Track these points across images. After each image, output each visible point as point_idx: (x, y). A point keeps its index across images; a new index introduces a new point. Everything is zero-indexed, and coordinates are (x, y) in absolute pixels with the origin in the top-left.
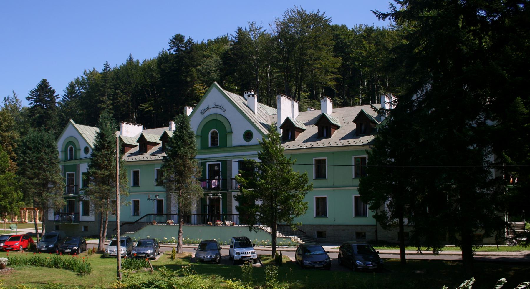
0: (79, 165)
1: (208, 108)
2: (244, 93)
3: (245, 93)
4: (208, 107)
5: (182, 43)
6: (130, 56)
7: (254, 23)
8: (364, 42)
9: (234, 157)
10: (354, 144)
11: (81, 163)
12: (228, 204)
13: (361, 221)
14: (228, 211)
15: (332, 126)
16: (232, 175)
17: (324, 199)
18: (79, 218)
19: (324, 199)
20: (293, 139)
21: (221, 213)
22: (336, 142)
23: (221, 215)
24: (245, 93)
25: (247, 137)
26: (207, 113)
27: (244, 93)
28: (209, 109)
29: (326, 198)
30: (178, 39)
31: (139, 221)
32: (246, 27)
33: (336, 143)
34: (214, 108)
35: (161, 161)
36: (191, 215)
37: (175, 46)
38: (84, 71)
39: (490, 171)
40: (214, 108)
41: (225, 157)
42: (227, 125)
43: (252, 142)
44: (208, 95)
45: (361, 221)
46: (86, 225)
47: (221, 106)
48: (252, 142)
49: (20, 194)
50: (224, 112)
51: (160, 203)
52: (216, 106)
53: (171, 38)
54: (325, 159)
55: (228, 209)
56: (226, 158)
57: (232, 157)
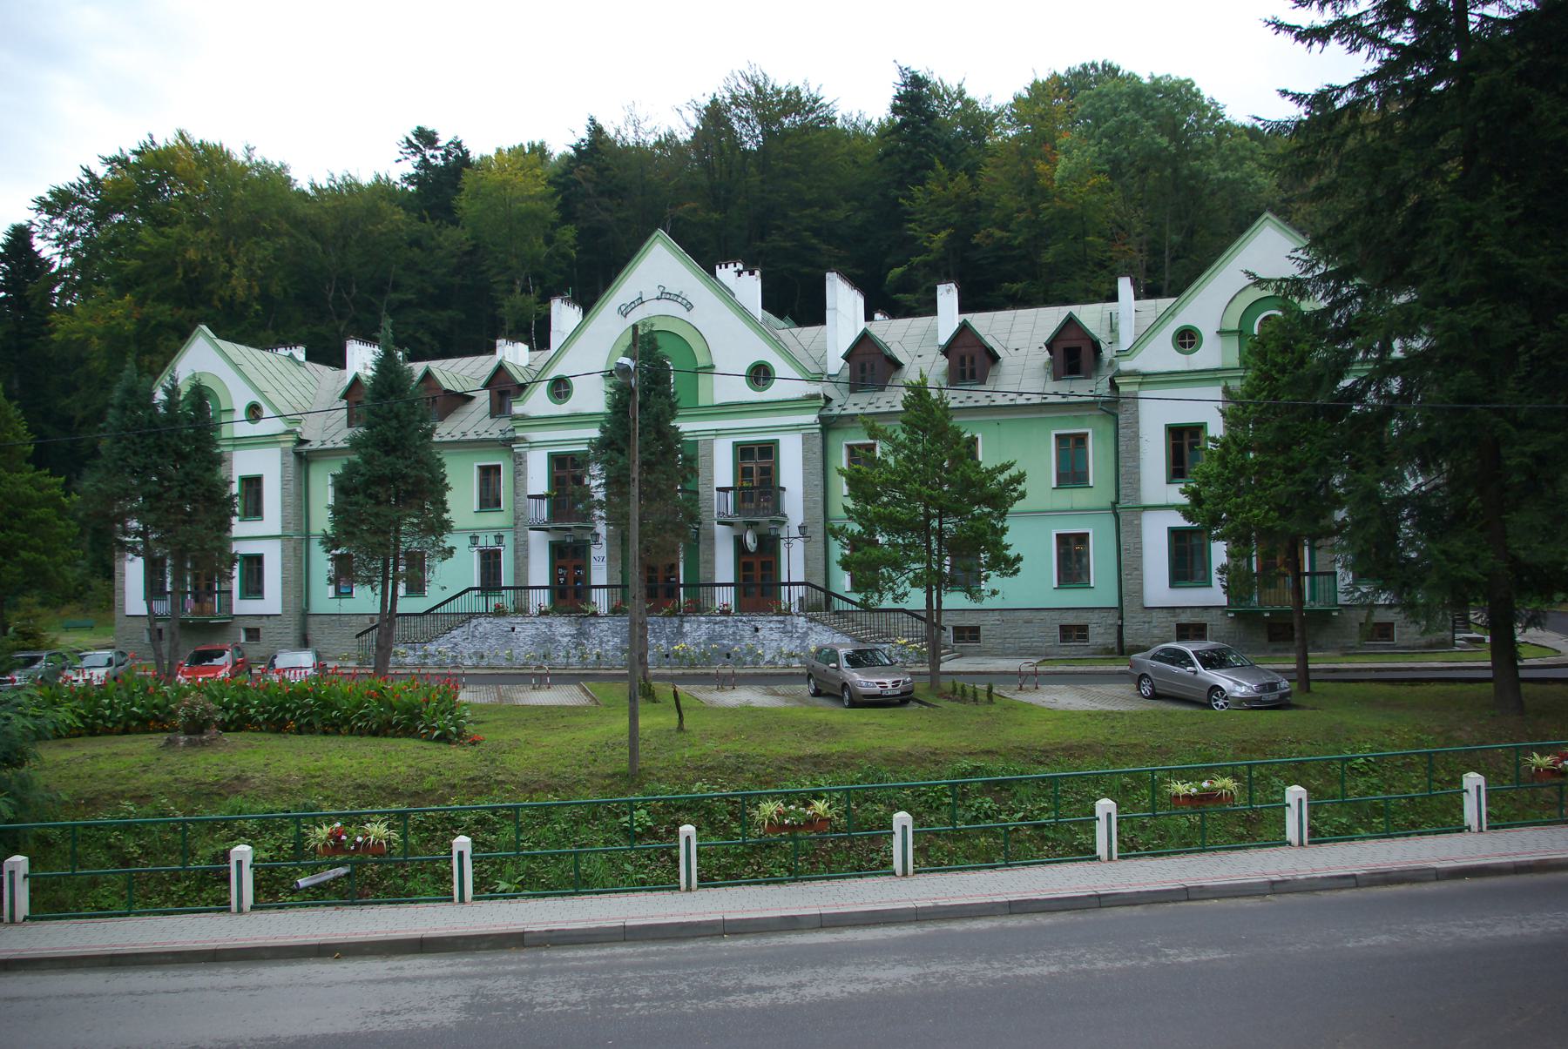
1: (641, 301)
4: (641, 298)
6: (593, 121)
13: (1074, 597)
17: (1082, 538)
18: (230, 605)
19: (1082, 538)
21: (681, 582)
23: (1307, 574)
26: (636, 316)
27: (717, 267)
28: (643, 302)
29: (1057, 535)
31: (439, 610)
34: (658, 299)
38: (1270, 30)
39: (446, 521)
42: (697, 347)
43: (767, 395)
45: (1074, 597)
46: (253, 624)
47: (679, 296)
50: (688, 310)
52: (664, 296)
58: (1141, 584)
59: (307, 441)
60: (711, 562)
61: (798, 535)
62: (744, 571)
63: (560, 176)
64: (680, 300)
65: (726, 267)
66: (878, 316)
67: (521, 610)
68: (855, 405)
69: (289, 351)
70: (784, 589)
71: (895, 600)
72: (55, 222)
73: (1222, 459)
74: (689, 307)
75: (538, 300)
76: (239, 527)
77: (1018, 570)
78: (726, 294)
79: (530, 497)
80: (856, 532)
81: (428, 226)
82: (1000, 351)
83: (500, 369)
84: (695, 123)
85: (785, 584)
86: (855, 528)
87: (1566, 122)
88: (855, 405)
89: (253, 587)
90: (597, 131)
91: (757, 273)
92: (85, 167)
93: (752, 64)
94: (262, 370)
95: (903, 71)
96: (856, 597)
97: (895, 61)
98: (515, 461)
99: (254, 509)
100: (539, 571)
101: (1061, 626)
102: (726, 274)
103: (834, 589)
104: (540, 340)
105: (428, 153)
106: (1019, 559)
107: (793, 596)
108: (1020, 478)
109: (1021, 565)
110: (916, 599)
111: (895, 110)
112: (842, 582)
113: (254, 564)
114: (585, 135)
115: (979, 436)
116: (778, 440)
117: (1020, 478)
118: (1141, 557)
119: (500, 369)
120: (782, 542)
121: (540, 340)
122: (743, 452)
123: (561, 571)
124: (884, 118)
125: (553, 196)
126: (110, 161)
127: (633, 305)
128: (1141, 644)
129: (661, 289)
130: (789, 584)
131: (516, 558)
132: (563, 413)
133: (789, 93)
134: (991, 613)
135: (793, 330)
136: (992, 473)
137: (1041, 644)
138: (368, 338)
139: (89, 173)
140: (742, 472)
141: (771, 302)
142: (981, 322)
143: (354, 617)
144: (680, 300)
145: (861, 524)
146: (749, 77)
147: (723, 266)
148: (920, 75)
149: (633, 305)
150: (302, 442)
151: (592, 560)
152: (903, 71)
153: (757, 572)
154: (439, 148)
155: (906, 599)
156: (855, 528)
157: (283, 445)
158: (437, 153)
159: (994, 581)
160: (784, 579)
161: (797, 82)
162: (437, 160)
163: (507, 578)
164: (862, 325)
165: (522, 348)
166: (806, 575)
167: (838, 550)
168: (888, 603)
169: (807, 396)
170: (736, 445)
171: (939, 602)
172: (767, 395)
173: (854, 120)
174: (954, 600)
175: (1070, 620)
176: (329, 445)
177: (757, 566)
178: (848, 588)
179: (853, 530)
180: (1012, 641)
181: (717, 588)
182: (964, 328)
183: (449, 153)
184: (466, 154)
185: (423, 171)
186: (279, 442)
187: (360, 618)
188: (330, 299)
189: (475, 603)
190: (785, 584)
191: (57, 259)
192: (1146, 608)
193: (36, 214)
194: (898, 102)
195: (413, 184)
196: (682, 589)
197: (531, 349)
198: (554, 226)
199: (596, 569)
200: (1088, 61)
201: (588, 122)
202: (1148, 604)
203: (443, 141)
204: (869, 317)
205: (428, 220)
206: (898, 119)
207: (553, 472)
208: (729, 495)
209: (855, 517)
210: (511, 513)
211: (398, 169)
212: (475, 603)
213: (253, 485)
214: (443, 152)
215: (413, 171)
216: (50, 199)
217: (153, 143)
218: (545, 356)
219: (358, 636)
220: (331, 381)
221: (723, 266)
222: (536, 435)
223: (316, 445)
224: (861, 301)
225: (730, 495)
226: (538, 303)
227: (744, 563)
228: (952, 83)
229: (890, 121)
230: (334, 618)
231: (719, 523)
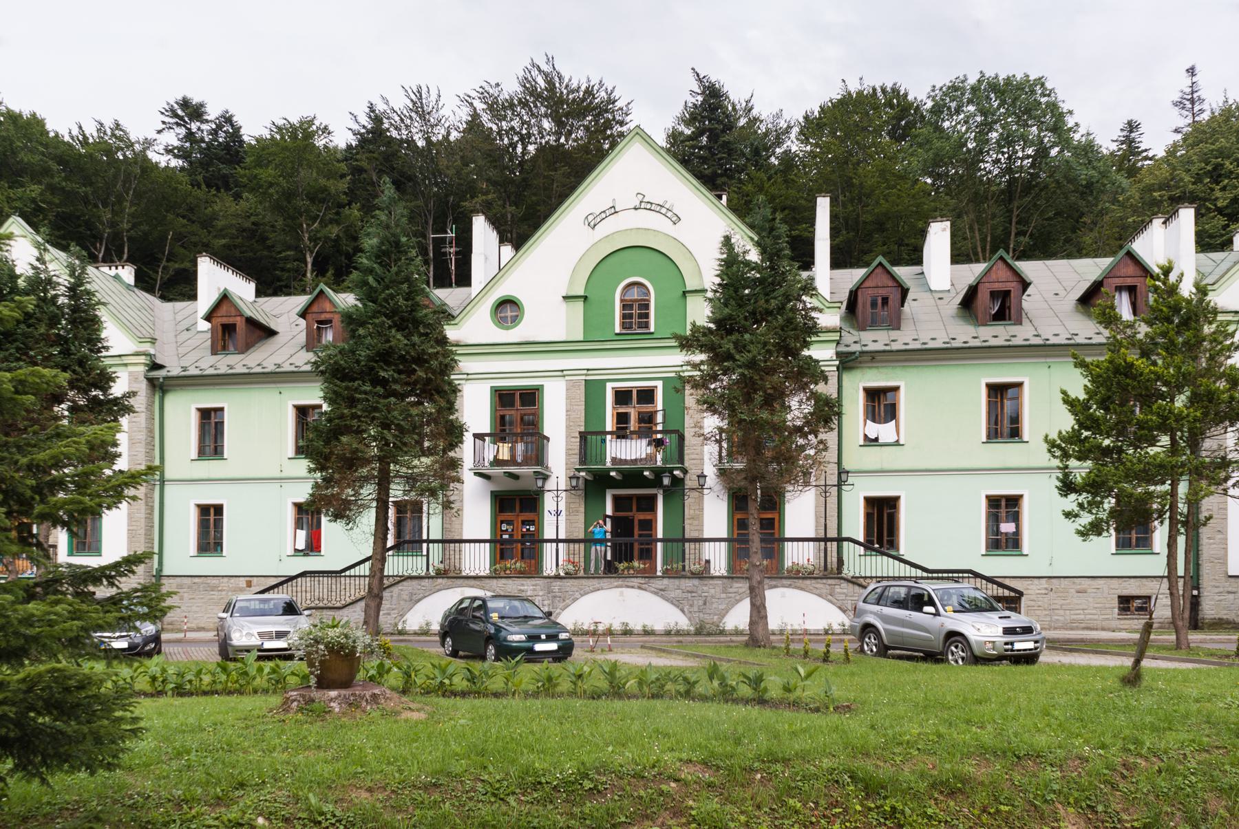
10: (999, 342)
21: (660, 535)
31: (352, 572)
34: (636, 209)
52: (645, 205)
58: (1226, 549)
64: (664, 211)
69: (113, 272)
73: (330, 420)
74: (677, 220)
87: (1238, 149)
93: (550, 57)
101: (1119, 597)
105: (194, 126)
107: (798, 555)
115: (902, 384)
118: (1226, 519)
122: (503, 398)
123: (504, 527)
127: (603, 215)
128: (1225, 617)
129: (640, 197)
130: (429, 541)
134: (1036, 581)
137: (1096, 617)
143: (226, 580)
144: (664, 211)
149: (603, 215)
150: (155, 366)
151: (546, 513)
154: (207, 121)
157: (131, 368)
158: (205, 127)
162: (203, 130)
175: (1131, 589)
176: (193, 371)
180: (1061, 612)
183: (219, 127)
184: (237, 130)
185: (188, 144)
186: (126, 365)
187: (233, 580)
192: (1231, 577)
196: (659, 545)
202: (1230, 573)
203: (213, 112)
215: (176, 143)
223: (175, 371)
230: (196, 580)
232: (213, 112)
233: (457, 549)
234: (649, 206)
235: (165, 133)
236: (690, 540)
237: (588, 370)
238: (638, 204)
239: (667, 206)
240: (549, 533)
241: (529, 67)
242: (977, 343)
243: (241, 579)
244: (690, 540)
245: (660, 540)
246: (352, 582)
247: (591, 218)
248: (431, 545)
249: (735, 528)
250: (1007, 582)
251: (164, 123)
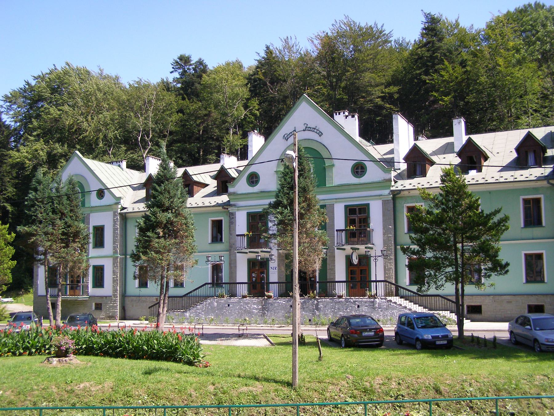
0: (89, 215)
2: (335, 114)
3: (336, 115)
4: (295, 130)
5: (189, 64)
7: (289, 38)
8: (446, 63)
9: (338, 200)
10: (522, 178)
11: (92, 212)
12: (328, 268)
14: (328, 277)
15: (427, 162)
16: (334, 225)
19: (539, 257)
20: (423, 174)
21: (318, 280)
22: (428, 183)
24: (336, 115)
25: (357, 172)
27: (335, 114)
29: (526, 255)
30: (184, 60)
32: (277, 45)
33: (429, 184)
34: (304, 130)
35: (221, 208)
36: (269, 283)
37: (179, 68)
40: (304, 130)
41: (324, 200)
43: (364, 180)
44: (295, 114)
46: (99, 301)
48: (364, 179)
49: (490, 265)
50: (320, 136)
51: (217, 269)
52: (307, 128)
53: (176, 59)
54: (408, 207)
55: (328, 274)
56: (326, 201)
57: (335, 200)
59: (126, 208)
60: (333, 270)
61: (381, 254)
62: (351, 275)
63: (252, 76)
65: (339, 114)
66: (420, 138)
67: (233, 295)
68: (410, 184)
70: (373, 285)
71: (437, 288)
72: (13, 106)
74: (320, 134)
75: (241, 137)
76: (93, 252)
77: (507, 271)
78: (341, 130)
79: (238, 235)
80: (416, 250)
81: (187, 102)
82: (489, 154)
83: (222, 169)
84: (320, 47)
85: (374, 281)
86: (415, 247)
88: (410, 184)
89: (99, 282)
90: (269, 51)
91: (356, 117)
92: (27, 81)
93: (346, 15)
94: (105, 173)
95: (427, 16)
96: (414, 288)
97: (422, 10)
98: (229, 216)
99: (99, 243)
100: (242, 275)
102: (340, 118)
103: (401, 284)
104: (243, 154)
106: (507, 264)
108: (506, 219)
109: (509, 268)
110: (449, 289)
111: (422, 35)
112: (405, 281)
113: (99, 271)
114: (263, 54)
116: (369, 204)
117: (506, 219)
119: (222, 169)
120: (372, 259)
121: (243, 154)
122: (350, 211)
124: (417, 39)
125: (247, 84)
126: (35, 78)
130: (376, 281)
131: (231, 267)
132: (255, 191)
133: (367, 29)
135: (375, 146)
136: (489, 217)
138: (157, 155)
139: (28, 84)
140: (350, 221)
141: (365, 133)
142: (478, 139)
144: (315, 131)
145: (418, 245)
146: (346, 22)
147: (338, 113)
148: (436, 16)
149: (291, 134)
151: (270, 268)
152: (427, 16)
153: (358, 276)
155: (442, 288)
156: (415, 247)
159: (495, 278)
160: (373, 278)
161: (371, 23)
163: (225, 278)
164: (412, 143)
165: (234, 159)
166: (385, 277)
167: (404, 260)
168: (432, 291)
169: (384, 180)
170: (346, 207)
171: (463, 290)
172: (364, 180)
173: (401, 42)
174: (469, 289)
175: (534, 302)
177: (358, 272)
178: (408, 283)
179: (414, 249)
181: (337, 284)
182: (470, 141)
188: (139, 140)
189: (208, 290)
190: (374, 281)
191: (13, 124)
193: (4, 103)
194: (424, 31)
195: (179, 83)
197: (238, 160)
198: (248, 100)
199: (271, 273)
200: (527, 3)
201: (265, 49)
203: (194, 60)
204: (416, 139)
205: (187, 100)
206: (425, 40)
207: (250, 223)
208: (343, 233)
209: (415, 242)
210: (228, 244)
211: (172, 76)
212: (208, 290)
213: (99, 231)
214: (194, 67)
216: (10, 96)
217: (56, 69)
218: (245, 162)
219: (149, 308)
220: (139, 177)
221: (338, 113)
222: (241, 203)
224: (411, 129)
225: (343, 233)
226: (241, 139)
227: (351, 270)
228: (452, 19)
229: (420, 41)
231: (337, 249)
232: (194, 60)
233: (333, 285)
234: (309, 129)
235: (174, 73)
236: (329, 282)
237: (336, 199)
238: (305, 128)
239: (317, 129)
240: (271, 280)
241: (334, 23)
242: (502, 180)
243: (154, 298)
244: (329, 282)
245: (318, 282)
246: (441, 306)
247: (286, 136)
248: (377, 283)
249: (350, 274)
250: (449, 298)
251: (173, 68)
